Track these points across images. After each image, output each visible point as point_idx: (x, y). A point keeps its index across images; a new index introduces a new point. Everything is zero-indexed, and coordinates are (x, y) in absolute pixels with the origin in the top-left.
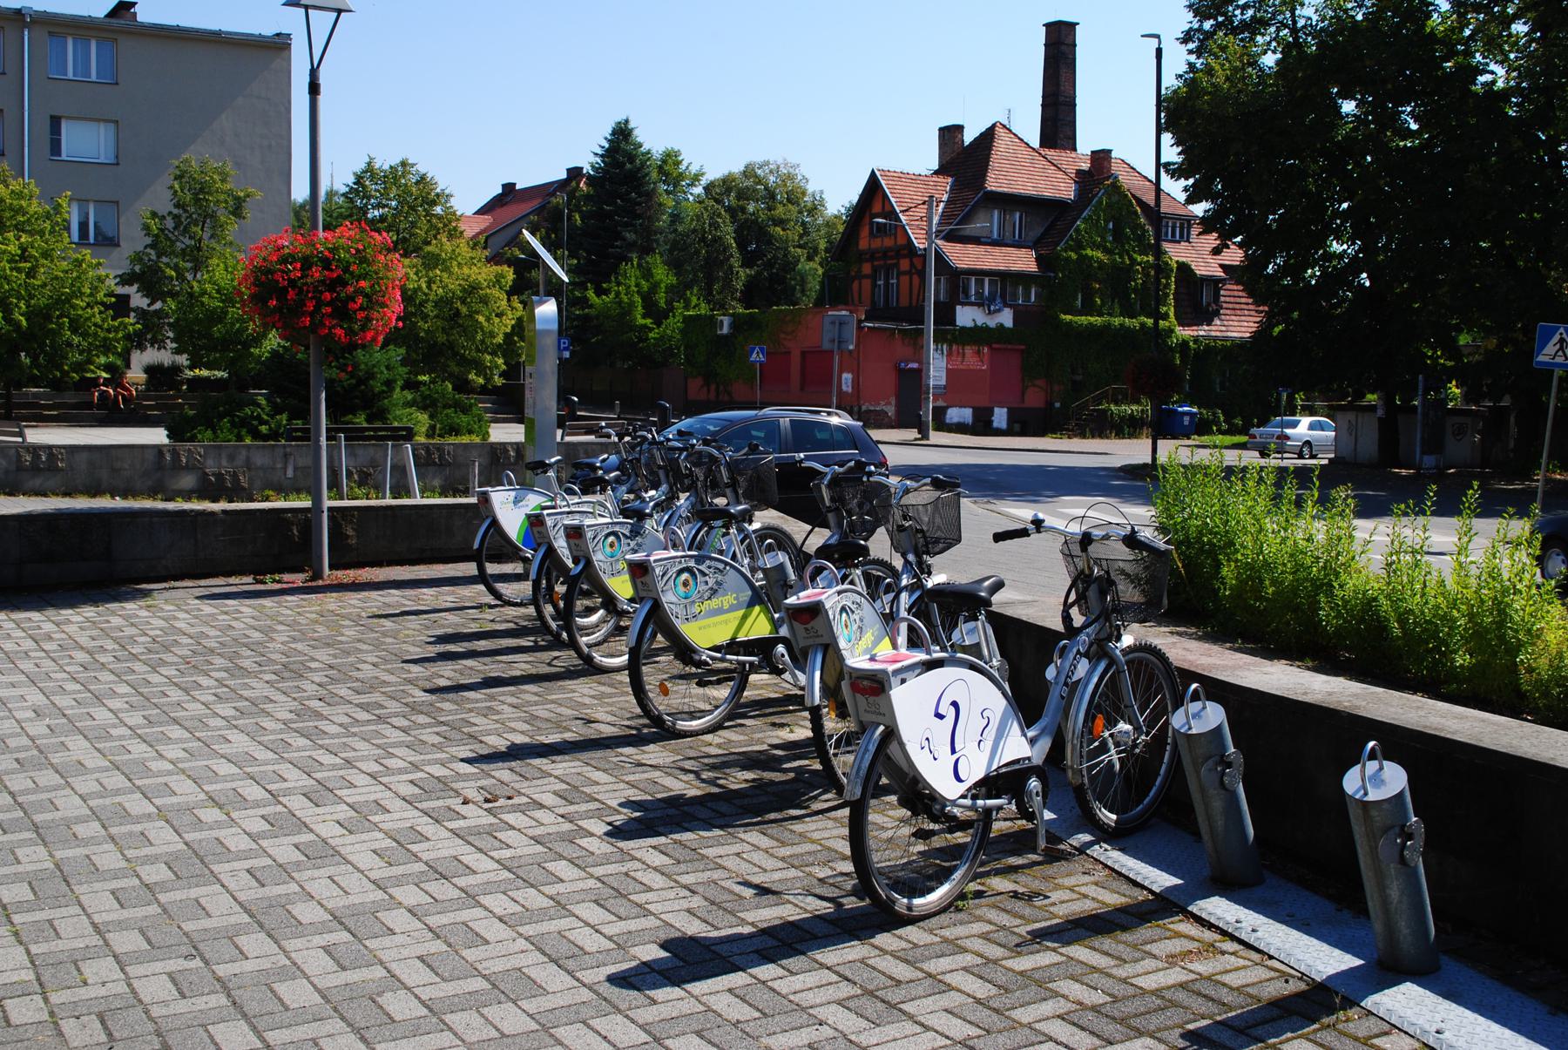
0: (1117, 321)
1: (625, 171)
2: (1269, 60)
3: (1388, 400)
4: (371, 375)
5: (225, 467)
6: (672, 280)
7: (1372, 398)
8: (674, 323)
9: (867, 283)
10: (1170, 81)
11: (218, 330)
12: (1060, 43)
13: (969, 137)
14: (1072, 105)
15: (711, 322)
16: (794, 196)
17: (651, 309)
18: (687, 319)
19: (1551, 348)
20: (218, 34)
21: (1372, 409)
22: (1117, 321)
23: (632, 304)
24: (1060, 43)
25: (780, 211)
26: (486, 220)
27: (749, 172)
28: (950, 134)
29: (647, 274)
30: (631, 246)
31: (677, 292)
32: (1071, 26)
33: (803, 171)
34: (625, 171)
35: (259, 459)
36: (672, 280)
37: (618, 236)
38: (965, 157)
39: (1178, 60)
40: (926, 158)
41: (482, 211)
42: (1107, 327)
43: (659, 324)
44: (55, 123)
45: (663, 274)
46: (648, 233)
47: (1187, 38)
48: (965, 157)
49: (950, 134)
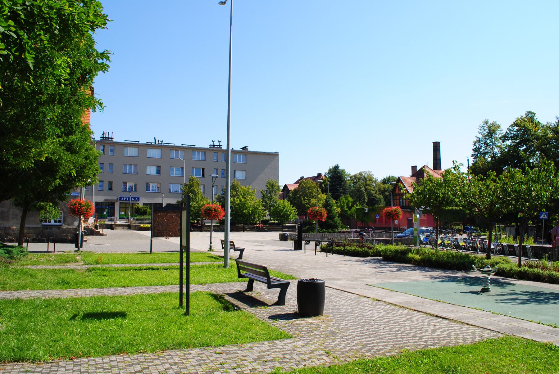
0: (454, 208)
1: (336, 175)
2: (489, 159)
3: (517, 225)
4: (337, 222)
5: (331, 237)
6: (352, 200)
7: (513, 224)
8: (353, 209)
9: (398, 201)
10: (470, 165)
11: (282, 214)
12: (436, 147)
13: (418, 169)
14: (440, 160)
15: (363, 209)
16: (371, 179)
17: (348, 207)
18: (357, 209)
19: (542, 216)
20: (265, 153)
21: (514, 226)
22: (454, 208)
23: (344, 205)
24: (436, 147)
25: (368, 182)
26: (297, 186)
27: (360, 174)
28: (414, 168)
29: (347, 199)
30: (341, 192)
31: (354, 203)
32: (439, 143)
33: (373, 173)
34: (336, 175)
35: (336, 236)
36: (352, 200)
37: (338, 190)
38: (418, 173)
39: (471, 162)
40: (409, 173)
41: (296, 183)
42: (452, 209)
43: (350, 210)
44: (235, 171)
45: (350, 199)
46: (345, 189)
47: (472, 156)
48: (418, 173)
49: (414, 168)
